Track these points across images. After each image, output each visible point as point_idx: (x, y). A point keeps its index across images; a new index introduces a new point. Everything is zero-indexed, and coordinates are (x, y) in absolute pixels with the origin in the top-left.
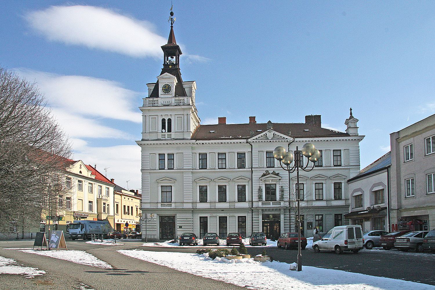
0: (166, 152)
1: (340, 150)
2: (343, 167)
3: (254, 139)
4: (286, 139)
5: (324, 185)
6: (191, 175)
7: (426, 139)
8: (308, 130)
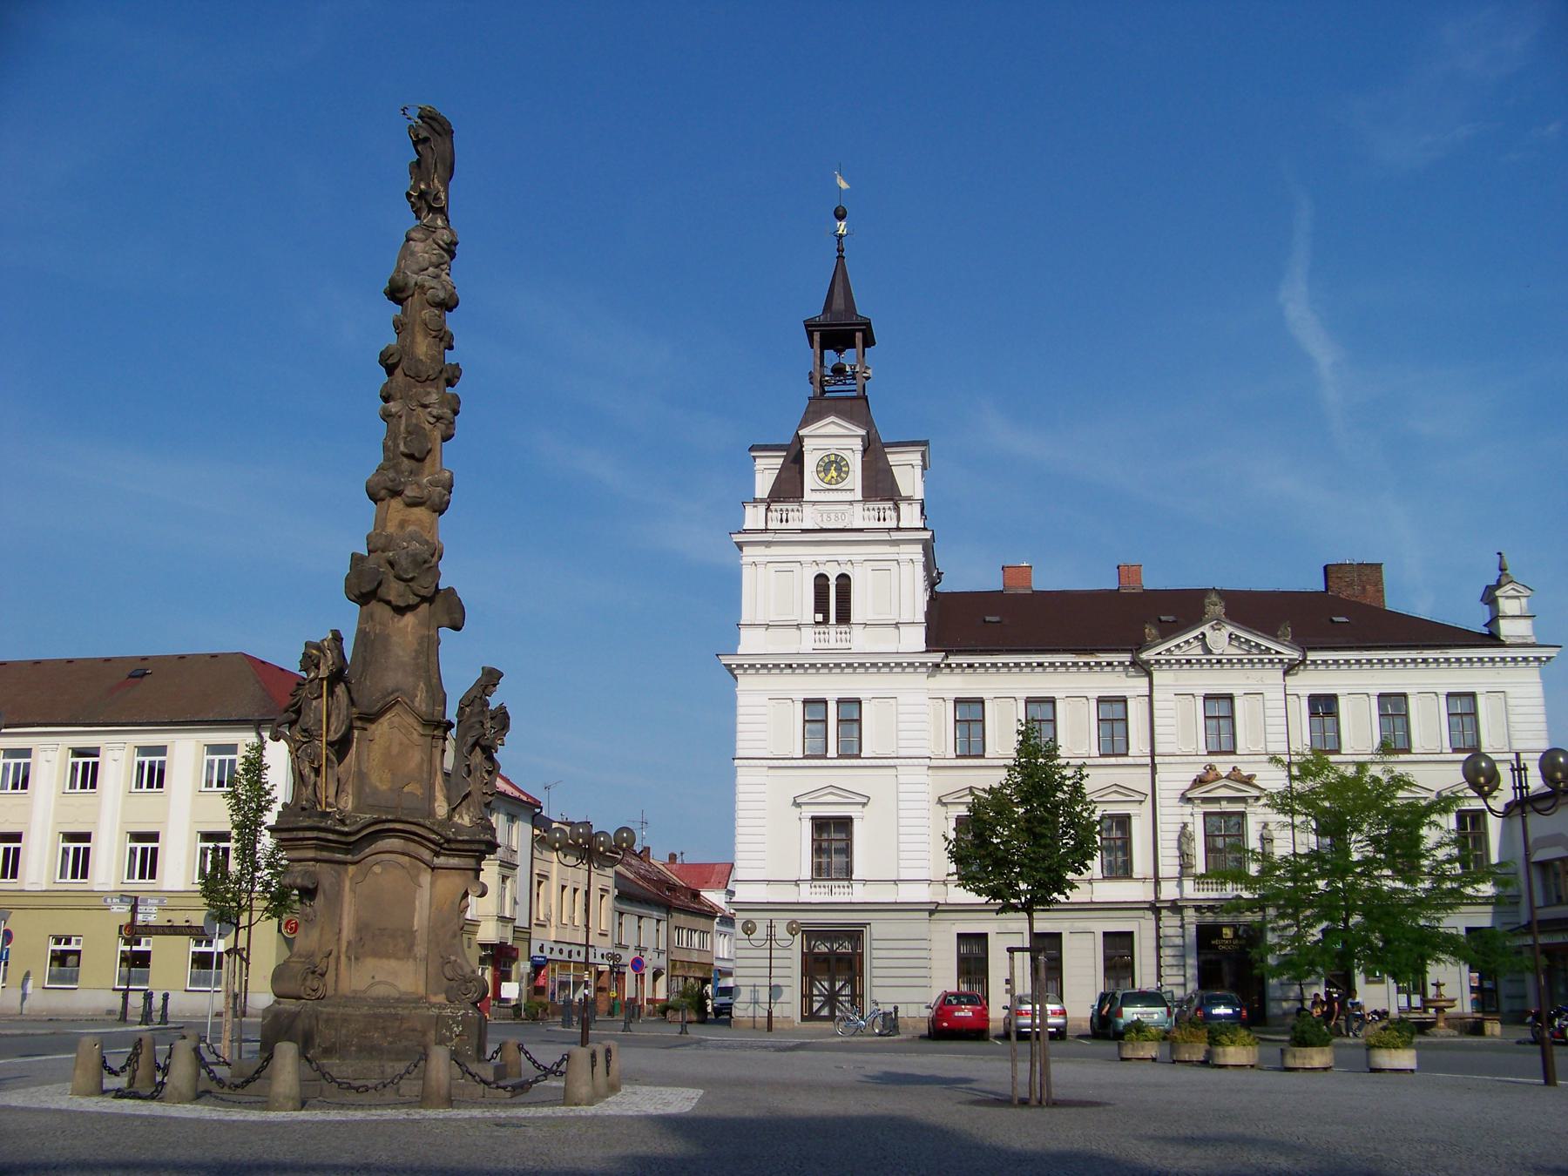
2: (868, 762)
3: (1160, 654)
8: (1344, 620)
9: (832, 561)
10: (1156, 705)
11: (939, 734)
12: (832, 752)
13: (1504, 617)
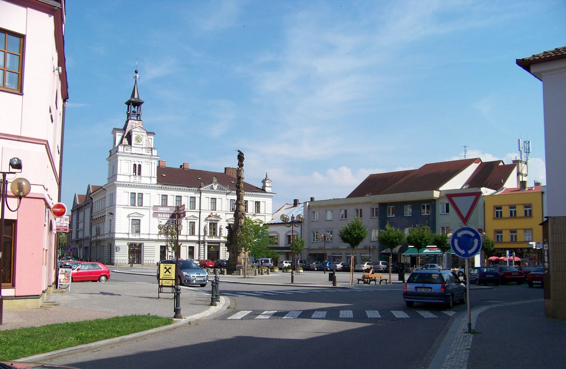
0: (137, 192)
2: (144, 208)
4: (226, 190)
7: (422, 206)
10: (202, 199)
11: (158, 201)
12: (136, 205)
13: (267, 187)
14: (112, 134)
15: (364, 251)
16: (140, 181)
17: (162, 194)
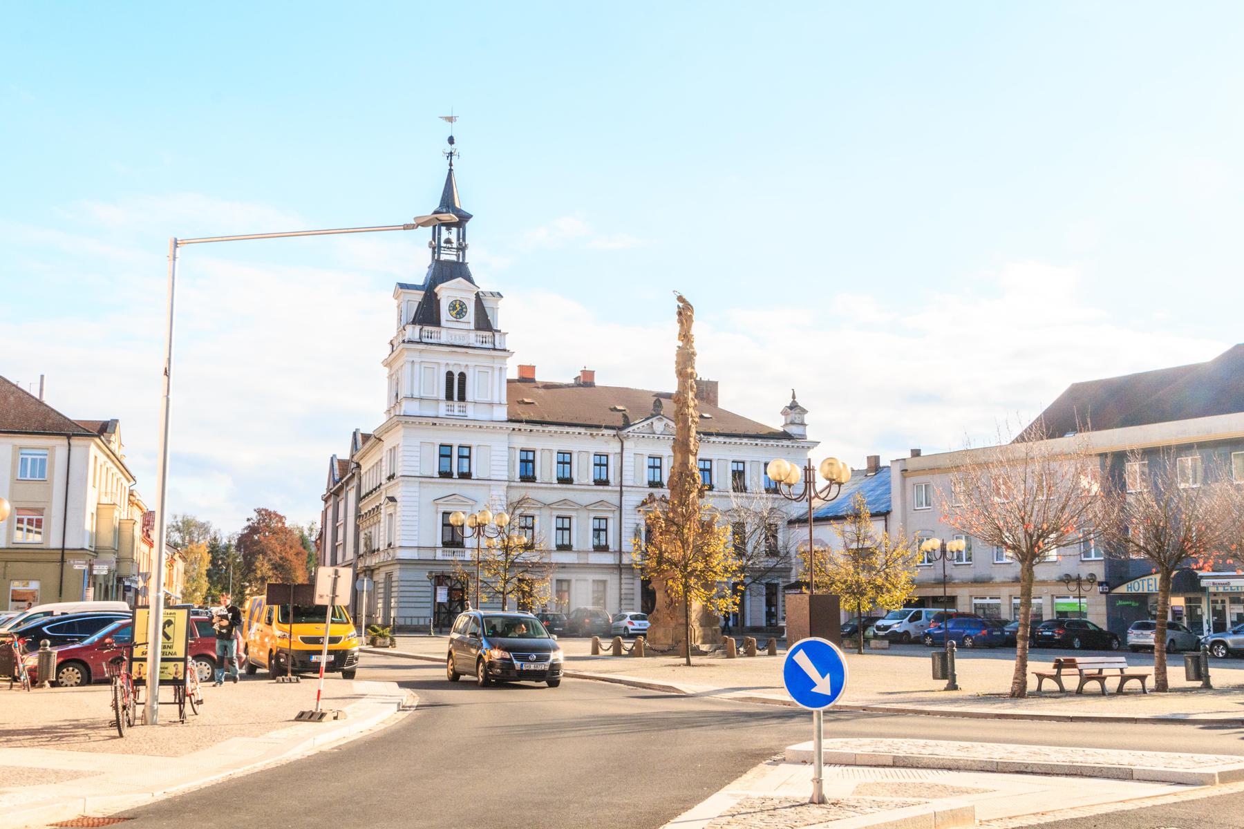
1: (451, 446)
5: (574, 521)
6: (417, 489)
9: (457, 363)
14: (393, 299)
15: (1063, 589)
16: (461, 414)
17: (732, 459)
